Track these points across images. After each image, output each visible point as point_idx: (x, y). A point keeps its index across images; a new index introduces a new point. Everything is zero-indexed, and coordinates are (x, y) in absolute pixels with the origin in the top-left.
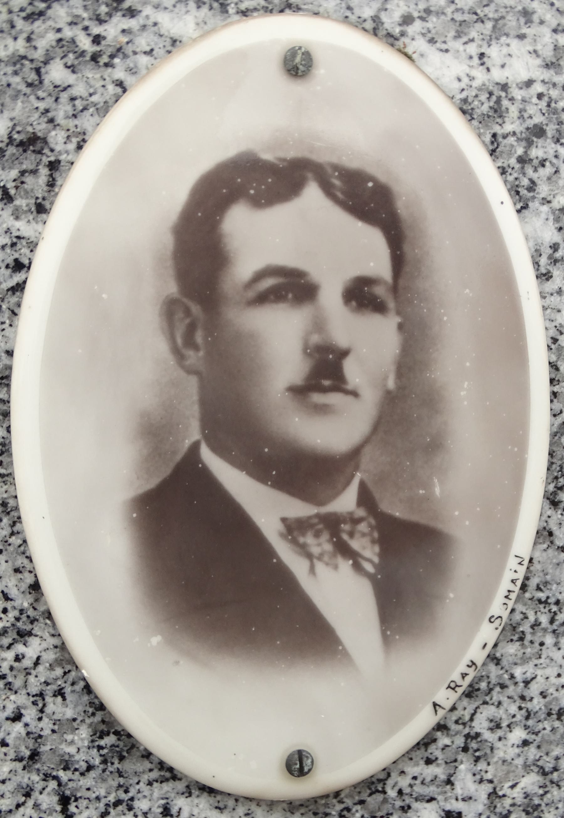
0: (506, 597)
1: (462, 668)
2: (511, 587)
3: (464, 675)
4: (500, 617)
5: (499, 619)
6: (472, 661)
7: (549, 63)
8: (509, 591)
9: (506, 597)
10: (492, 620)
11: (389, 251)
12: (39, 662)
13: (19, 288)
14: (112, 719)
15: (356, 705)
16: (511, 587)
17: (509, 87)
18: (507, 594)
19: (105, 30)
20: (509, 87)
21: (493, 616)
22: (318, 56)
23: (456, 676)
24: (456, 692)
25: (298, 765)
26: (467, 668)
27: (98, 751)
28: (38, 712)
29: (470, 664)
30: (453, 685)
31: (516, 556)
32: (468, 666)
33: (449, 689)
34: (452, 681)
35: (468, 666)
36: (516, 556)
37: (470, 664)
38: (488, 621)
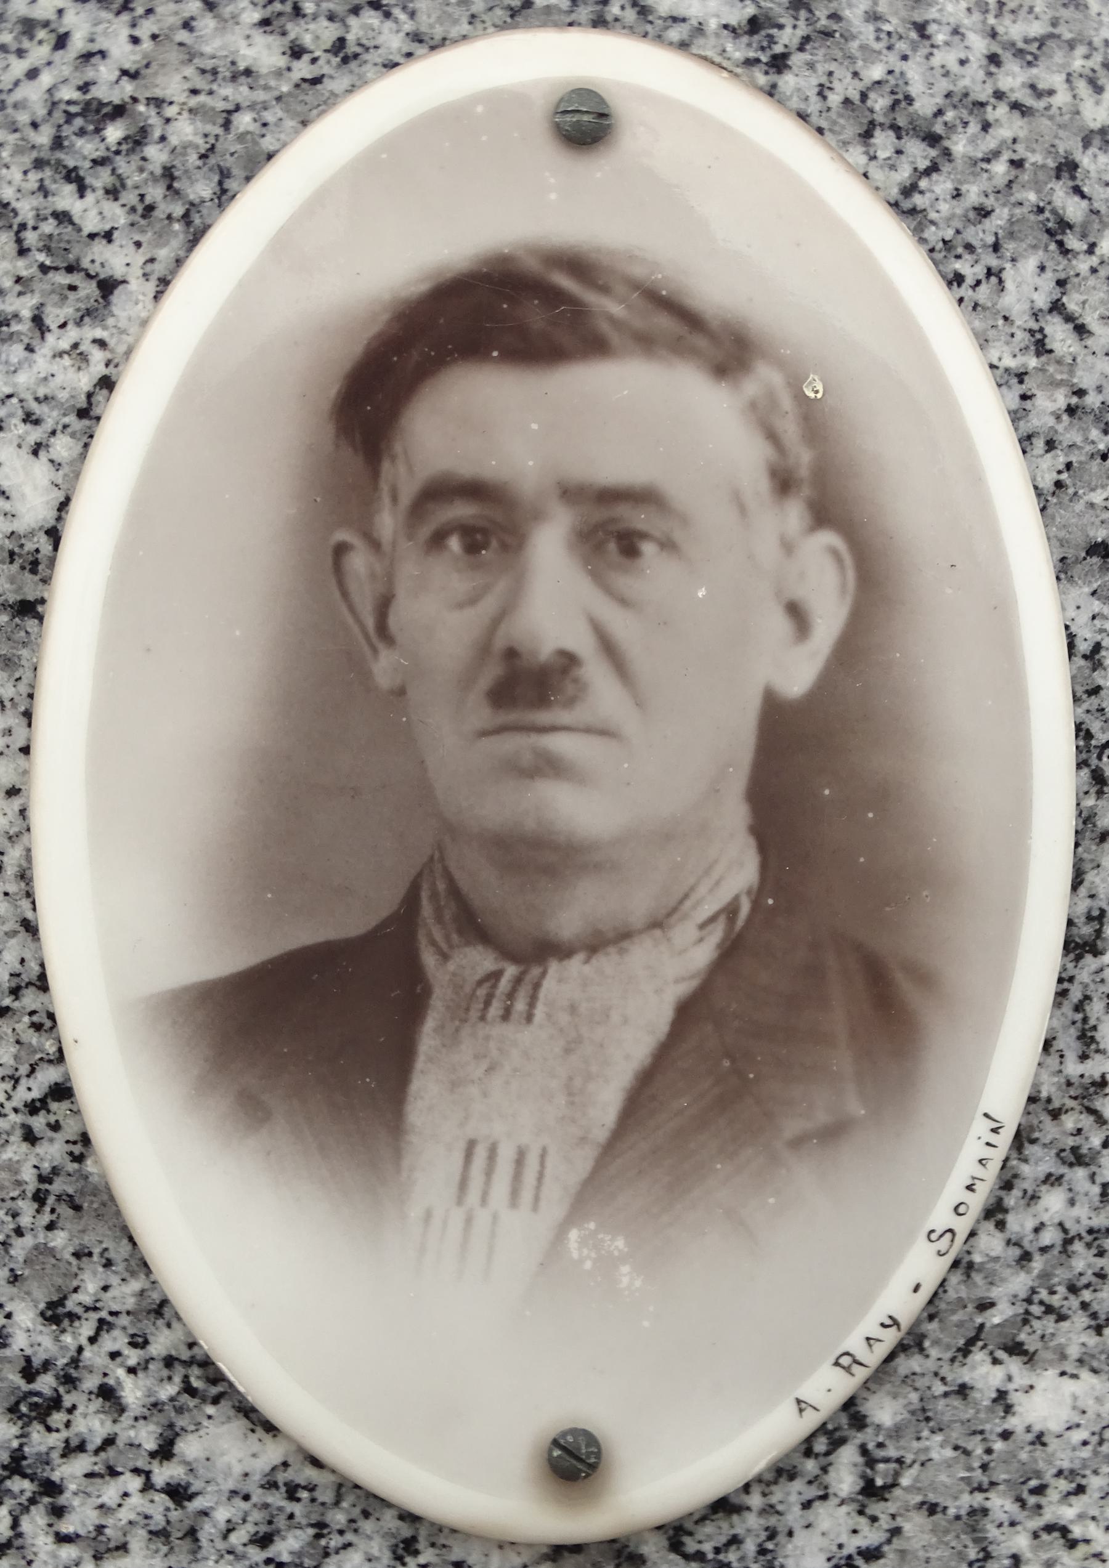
1: (869, 1325)
4: (950, 1230)
5: (949, 1235)
8: (974, 1178)
10: (934, 1236)
12: (260, 1432)
13: (30, 609)
14: (39, 640)
16: (979, 1171)
17: (161, 1462)
18: (969, 1182)
19: (194, 92)
20: (161, 1462)
21: (932, 1231)
22: (621, 106)
23: (855, 1343)
26: (881, 1329)
29: (888, 1322)
32: (883, 1325)
34: (847, 1354)
35: (883, 1325)
38: (957, 1230)
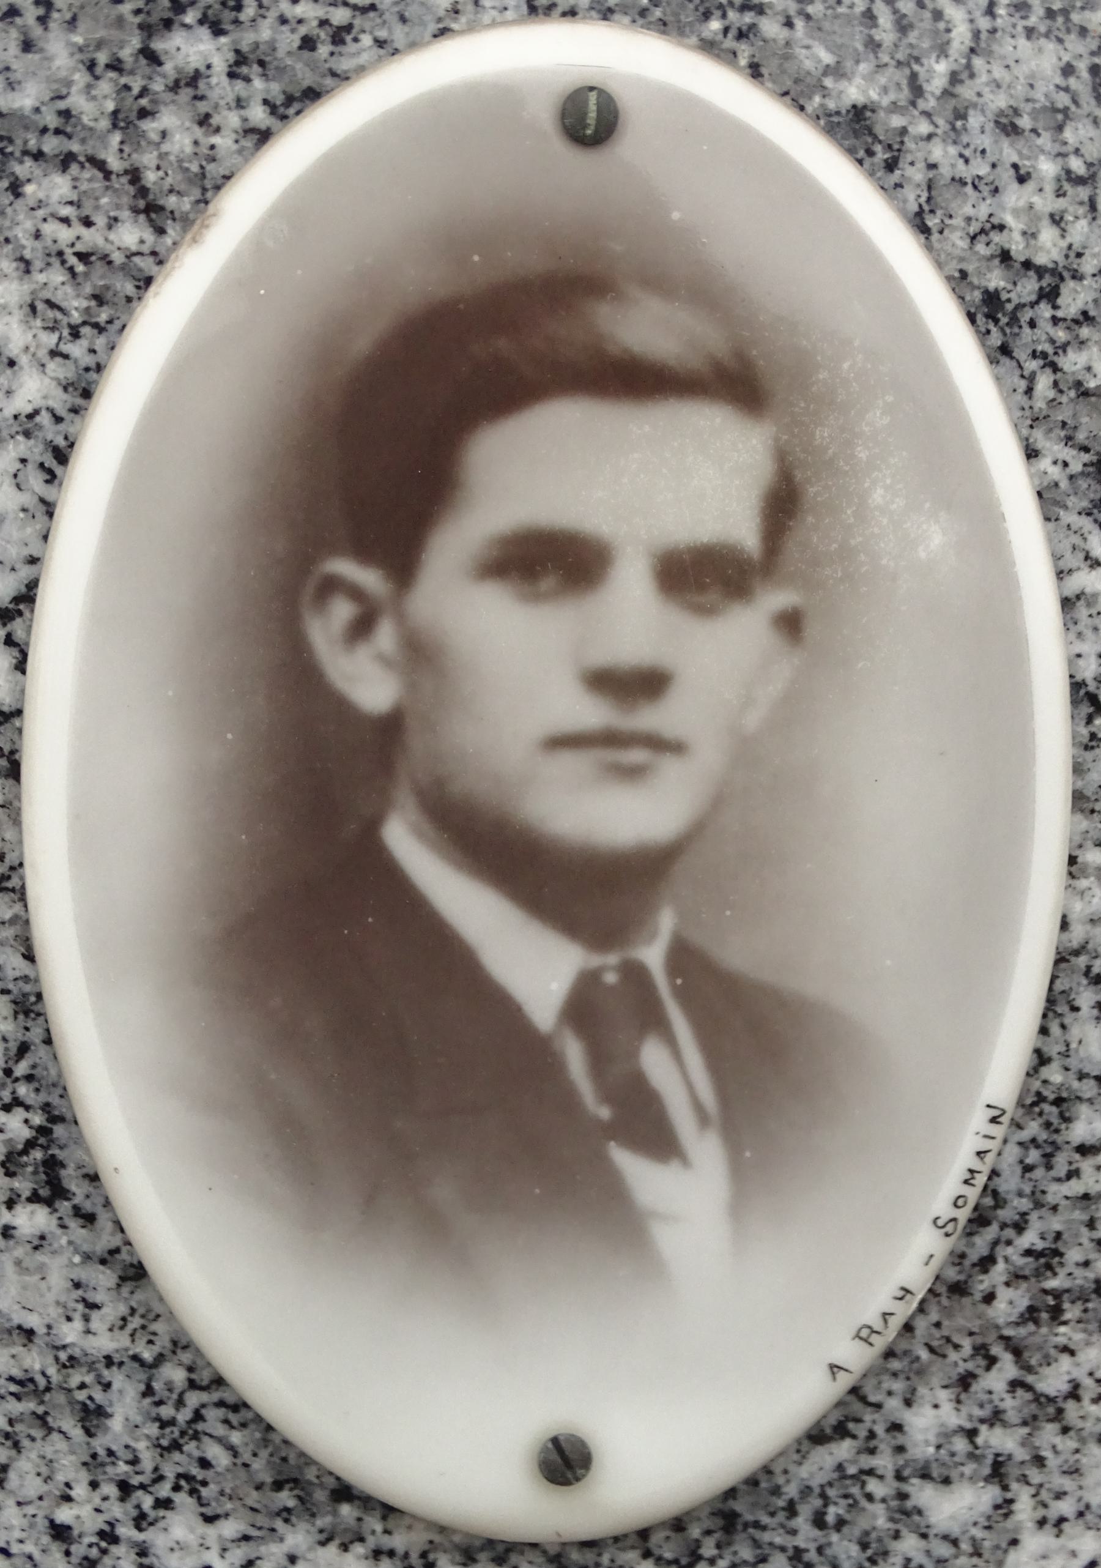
0: (966, 1182)
2: (976, 1165)
3: (886, 1316)
6: (903, 1289)
7: (106, 1255)
8: (971, 1171)
9: (966, 1182)
11: (672, 400)
15: (708, 1337)
18: (968, 1176)
24: (871, 1344)
25: (565, 1462)
27: (962, 82)
28: (41, 44)
29: (901, 1294)
30: (864, 1333)
31: (988, 1106)
33: (857, 1339)
36: (988, 1106)
37: (901, 1294)
